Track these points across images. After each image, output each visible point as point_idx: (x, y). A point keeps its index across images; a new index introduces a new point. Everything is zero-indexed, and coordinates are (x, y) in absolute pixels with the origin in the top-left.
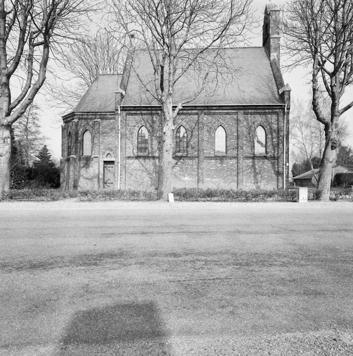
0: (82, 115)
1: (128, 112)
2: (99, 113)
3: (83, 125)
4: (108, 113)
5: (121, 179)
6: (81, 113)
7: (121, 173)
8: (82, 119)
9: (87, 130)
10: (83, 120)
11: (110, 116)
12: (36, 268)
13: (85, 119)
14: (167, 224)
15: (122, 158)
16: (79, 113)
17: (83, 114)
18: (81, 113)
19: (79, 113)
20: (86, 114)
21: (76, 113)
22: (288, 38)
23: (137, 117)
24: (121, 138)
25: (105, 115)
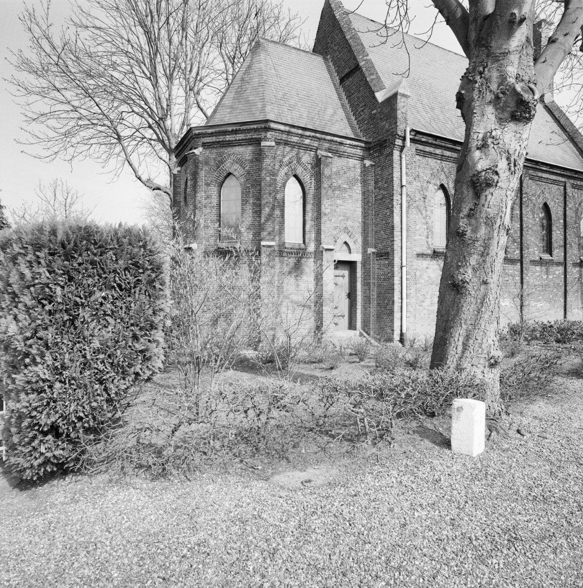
0: (289, 133)
1: (421, 147)
2: (329, 138)
3: (286, 159)
4: (348, 142)
5: (409, 307)
6: (287, 128)
7: (409, 292)
8: (286, 143)
9: (230, 174)
10: (288, 149)
11: (349, 150)
12: (114, 369)
13: (293, 145)
14: (54, 232)
15: (410, 256)
16: (282, 128)
17: (293, 130)
18: (287, 128)
19: (282, 128)
20: (300, 132)
21: (273, 125)
22: (112, 138)
23: (432, 162)
24: (408, 207)
25: (341, 144)
